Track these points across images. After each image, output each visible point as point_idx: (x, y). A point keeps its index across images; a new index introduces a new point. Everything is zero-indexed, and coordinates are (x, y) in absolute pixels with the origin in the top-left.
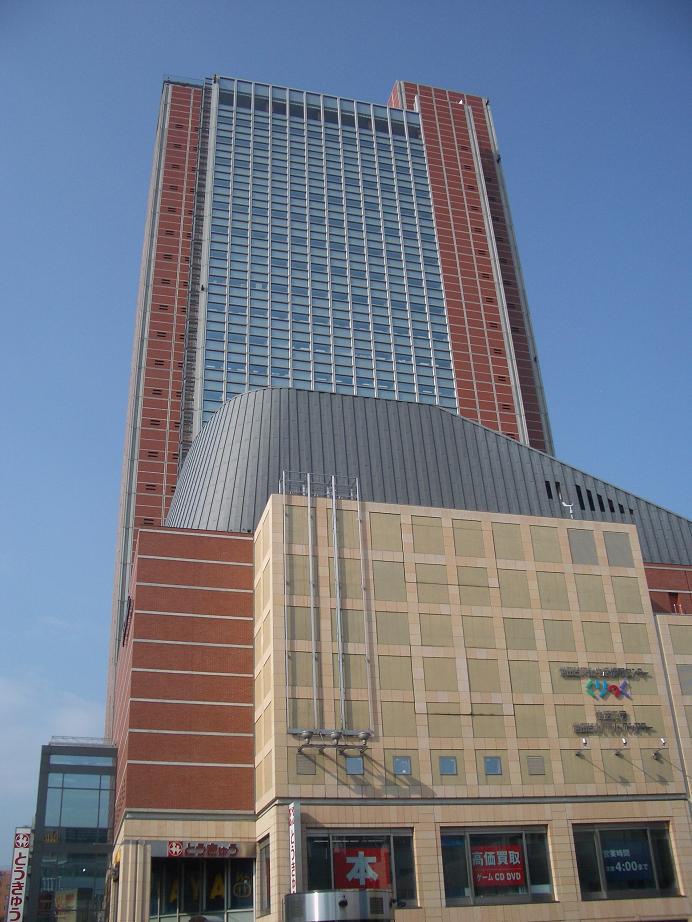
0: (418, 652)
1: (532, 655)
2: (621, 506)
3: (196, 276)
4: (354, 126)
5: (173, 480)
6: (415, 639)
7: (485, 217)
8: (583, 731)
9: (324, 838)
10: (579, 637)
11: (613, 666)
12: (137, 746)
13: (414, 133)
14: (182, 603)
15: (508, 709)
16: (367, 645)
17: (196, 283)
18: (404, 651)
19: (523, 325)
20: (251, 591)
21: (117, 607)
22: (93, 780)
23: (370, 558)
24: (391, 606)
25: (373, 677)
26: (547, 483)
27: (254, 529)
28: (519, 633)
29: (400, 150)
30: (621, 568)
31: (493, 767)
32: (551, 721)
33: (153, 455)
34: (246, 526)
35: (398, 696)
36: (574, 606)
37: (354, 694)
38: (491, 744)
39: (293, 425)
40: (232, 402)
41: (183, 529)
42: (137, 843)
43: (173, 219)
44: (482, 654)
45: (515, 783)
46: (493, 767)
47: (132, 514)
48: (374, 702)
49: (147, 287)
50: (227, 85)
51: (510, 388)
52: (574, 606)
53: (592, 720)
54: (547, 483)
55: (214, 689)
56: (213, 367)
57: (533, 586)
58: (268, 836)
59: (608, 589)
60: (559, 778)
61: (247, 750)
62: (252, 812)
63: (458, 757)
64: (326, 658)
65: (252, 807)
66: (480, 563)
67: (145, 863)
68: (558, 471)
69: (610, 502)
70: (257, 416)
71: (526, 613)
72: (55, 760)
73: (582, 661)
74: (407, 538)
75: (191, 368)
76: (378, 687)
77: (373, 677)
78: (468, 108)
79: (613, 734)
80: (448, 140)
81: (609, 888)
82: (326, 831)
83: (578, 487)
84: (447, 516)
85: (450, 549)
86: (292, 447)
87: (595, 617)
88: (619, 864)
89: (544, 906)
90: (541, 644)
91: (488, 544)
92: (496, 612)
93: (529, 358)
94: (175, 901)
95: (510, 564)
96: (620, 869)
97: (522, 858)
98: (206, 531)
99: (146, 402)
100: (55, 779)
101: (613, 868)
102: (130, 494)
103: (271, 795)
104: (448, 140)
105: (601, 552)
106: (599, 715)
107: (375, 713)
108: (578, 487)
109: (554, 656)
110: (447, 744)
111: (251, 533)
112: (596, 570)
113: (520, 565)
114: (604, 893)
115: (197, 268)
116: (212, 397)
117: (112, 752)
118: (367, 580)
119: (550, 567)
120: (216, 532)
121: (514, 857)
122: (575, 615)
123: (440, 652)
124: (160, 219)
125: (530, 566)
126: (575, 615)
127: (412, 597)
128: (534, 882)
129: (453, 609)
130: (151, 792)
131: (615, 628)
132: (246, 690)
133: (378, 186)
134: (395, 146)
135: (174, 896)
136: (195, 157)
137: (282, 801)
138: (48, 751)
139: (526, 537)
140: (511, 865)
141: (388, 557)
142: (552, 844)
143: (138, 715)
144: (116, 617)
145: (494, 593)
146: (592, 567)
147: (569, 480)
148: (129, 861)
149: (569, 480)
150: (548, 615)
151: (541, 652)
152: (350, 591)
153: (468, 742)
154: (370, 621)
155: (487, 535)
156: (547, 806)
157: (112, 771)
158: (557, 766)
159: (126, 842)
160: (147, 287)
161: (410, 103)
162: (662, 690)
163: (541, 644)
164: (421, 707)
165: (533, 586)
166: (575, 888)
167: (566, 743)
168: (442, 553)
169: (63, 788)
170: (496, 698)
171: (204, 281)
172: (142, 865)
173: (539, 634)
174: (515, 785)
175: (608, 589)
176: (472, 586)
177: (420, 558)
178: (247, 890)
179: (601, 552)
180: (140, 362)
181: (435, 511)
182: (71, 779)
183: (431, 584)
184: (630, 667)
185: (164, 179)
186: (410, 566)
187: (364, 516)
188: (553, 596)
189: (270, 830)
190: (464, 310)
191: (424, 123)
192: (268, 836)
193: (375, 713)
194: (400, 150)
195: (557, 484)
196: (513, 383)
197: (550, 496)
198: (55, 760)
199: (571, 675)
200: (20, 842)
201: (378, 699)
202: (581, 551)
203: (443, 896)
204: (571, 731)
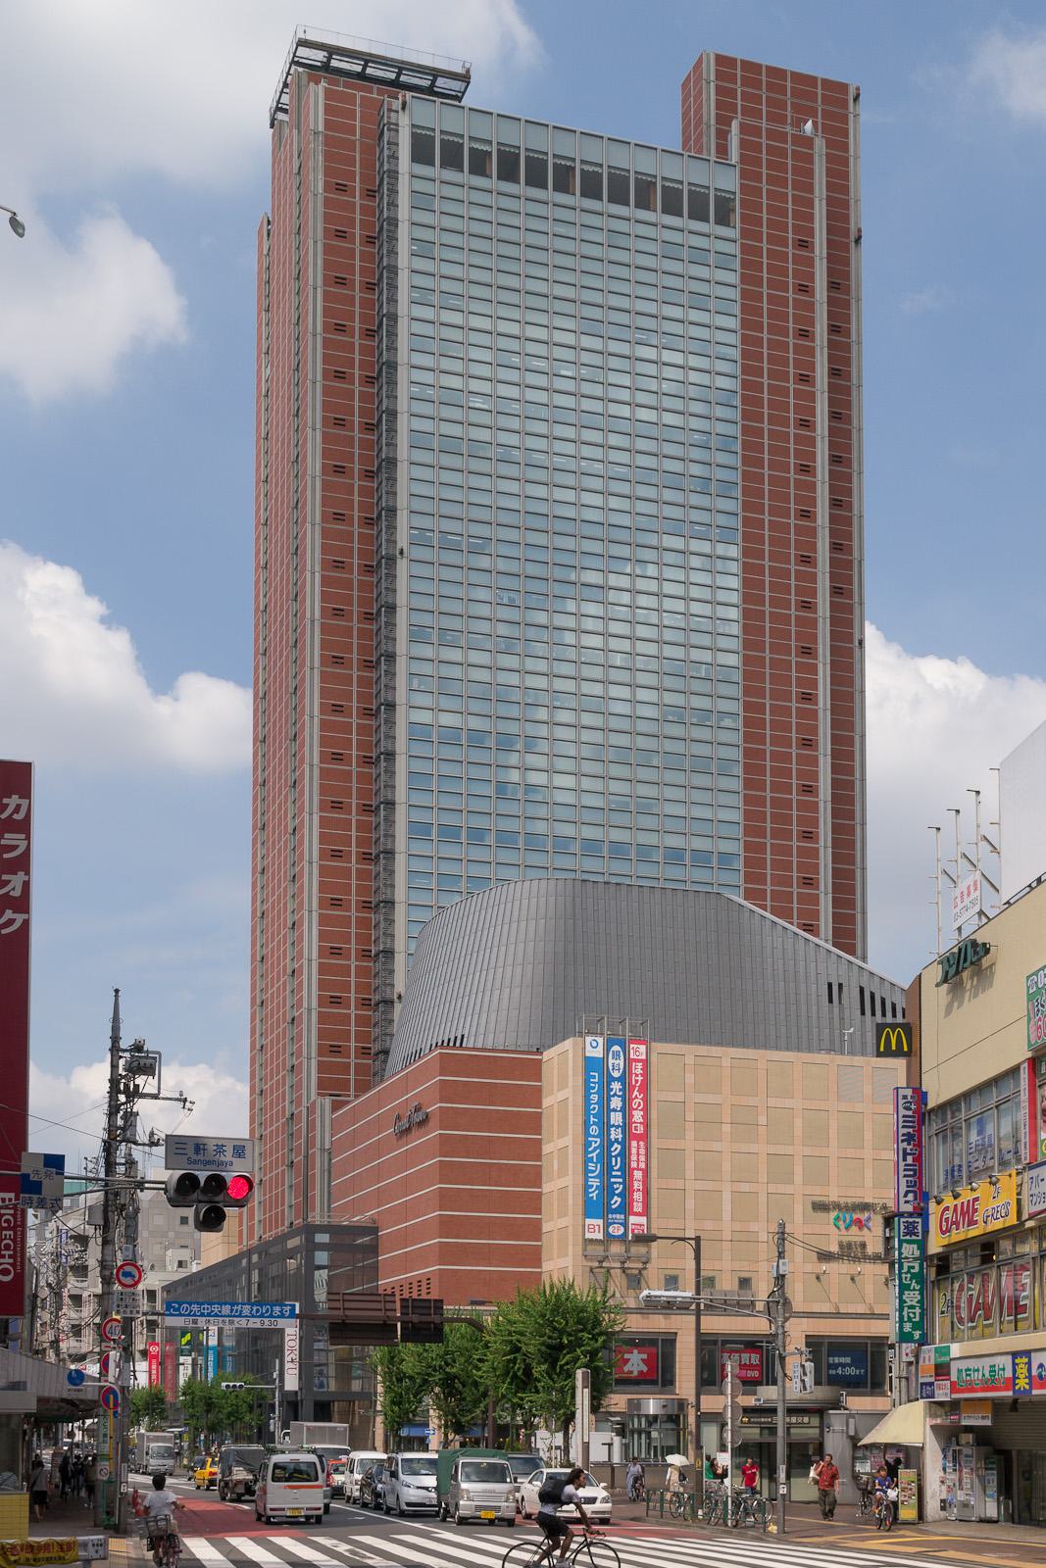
6: (690, 1173)
8: (825, 1256)
11: (861, 1200)
18: (680, 1184)
26: (830, 985)
44: (745, 1187)
54: (830, 985)
55: (507, 1202)
71: (788, 1150)
73: (834, 1195)
74: (690, 1078)
87: (851, 1153)
97: (761, 1360)
123: (709, 1186)
127: (690, 1134)
150: (808, 1151)
167: (809, 1268)
170: (754, 1227)
177: (700, 1098)
197: (831, 1001)
199: (820, 1207)
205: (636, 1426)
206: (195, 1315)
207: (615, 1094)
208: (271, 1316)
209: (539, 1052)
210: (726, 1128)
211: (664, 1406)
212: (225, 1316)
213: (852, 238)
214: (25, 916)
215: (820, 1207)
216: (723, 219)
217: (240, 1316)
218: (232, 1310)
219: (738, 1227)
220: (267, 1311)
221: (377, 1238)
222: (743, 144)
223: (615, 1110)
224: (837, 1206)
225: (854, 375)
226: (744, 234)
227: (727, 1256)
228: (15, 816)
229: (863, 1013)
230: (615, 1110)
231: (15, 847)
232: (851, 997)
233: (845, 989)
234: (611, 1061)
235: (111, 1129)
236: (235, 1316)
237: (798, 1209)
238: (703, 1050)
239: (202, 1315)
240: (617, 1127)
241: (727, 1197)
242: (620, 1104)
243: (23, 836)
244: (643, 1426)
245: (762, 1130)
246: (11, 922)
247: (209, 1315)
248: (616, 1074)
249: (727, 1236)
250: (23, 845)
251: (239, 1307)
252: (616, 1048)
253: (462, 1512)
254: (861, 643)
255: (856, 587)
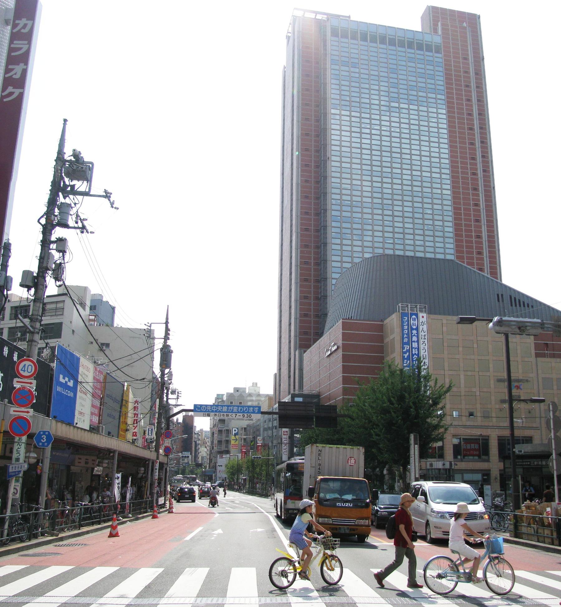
15: (478, 394)
19: (482, 84)
26: (498, 295)
44: (469, 373)
45: (479, 421)
51: (475, 148)
54: (498, 295)
93: (490, 187)
97: (479, 447)
121: (477, 446)
140: (475, 449)
162: (536, 387)
167: (497, 406)
184: (524, 378)
196: (484, 239)
206: (209, 411)
207: (414, 335)
208: (248, 412)
209: (382, 321)
210: (461, 349)
212: (224, 412)
214: (21, 90)
216: (437, 52)
217: (232, 412)
218: (228, 409)
220: (246, 410)
221: (319, 399)
222: (443, 29)
223: (414, 342)
226: (445, 55)
228: (23, 31)
229: (512, 305)
230: (414, 342)
231: (20, 49)
232: (507, 300)
234: (412, 322)
235: (49, 214)
236: (229, 412)
237: (492, 382)
239: (213, 411)
240: (415, 348)
241: (462, 377)
242: (416, 339)
243: (26, 42)
246: (11, 94)
247: (216, 411)
248: (414, 327)
249: (463, 394)
250: (25, 48)
251: (232, 408)
252: (414, 317)
254: (494, 188)
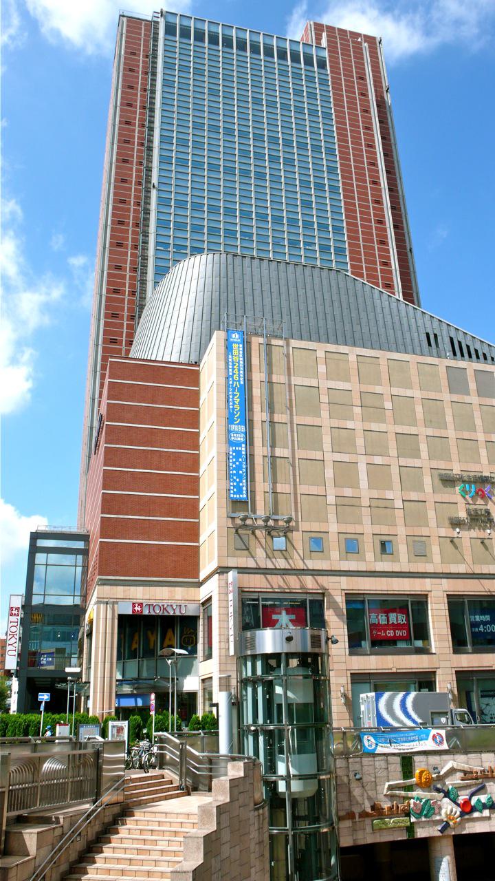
0: (330, 457)
1: (417, 463)
2: (484, 355)
3: (149, 176)
4: (274, 57)
5: (131, 335)
6: (327, 446)
7: (375, 135)
8: (456, 523)
9: (253, 600)
10: (454, 450)
11: (480, 474)
12: (107, 527)
13: (322, 65)
14: (141, 414)
16: (290, 450)
17: (148, 181)
18: (318, 455)
20: (198, 409)
21: (87, 432)
22: (69, 559)
23: (293, 383)
24: (308, 420)
25: (294, 475)
26: (428, 335)
27: (200, 360)
28: (407, 444)
29: (310, 79)
30: (487, 399)
31: (384, 547)
32: (431, 514)
33: (115, 316)
34: (193, 359)
35: (314, 490)
36: (450, 426)
37: (280, 488)
38: (384, 530)
39: (230, 281)
40: (178, 266)
41: (143, 360)
42: (107, 604)
43: (129, 130)
44: (378, 460)
46: (384, 547)
47: (101, 327)
48: (295, 494)
49: (110, 184)
50: (171, 19)
52: (450, 426)
53: (463, 514)
54: (428, 335)
55: (167, 484)
56: (162, 248)
57: (419, 409)
58: (210, 599)
59: (477, 414)
60: (437, 558)
61: (193, 532)
62: (196, 580)
63: (359, 540)
64: (258, 460)
65: (197, 576)
66: (378, 389)
67: (113, 619)
68: (436, 324)
69: (476, 351)
70: (202, 274)
71: (413, 430)
72: (42, 543)
73: (457, 469)
74: (322, 369)
75: (145, 249)
76: (298, 483)
77: (294, 475)
78: (365, 45)
79: (479, 529)
80: (348, 73)
81: (474, 644)
82: (257, 594)
83: (451, 339)
84: (353, 353)
85: (355, 378)
86: (229, 284)
87: (466, 435)
88: (482, 626)
89: (425, 657)
90: (424, 453)
91: (385, 376)
92: (391, 428)
94: (136, 649)
95: (402, 392)
96: (482, 630)
97: (408, 620)
98: (162, 362)
99: (109, 275)
100: (40, 558)
101: (477, 629)
102: (97, 346)
103: (214, 565)
104: (348, 73)
105: (472, 386)
106: (468, 511)
107: (296, 503)
108: (451, 339)
109: (435, 464)
110: (350, 528)
111: (197, 364)
112: (467, 399)
113: (409, 393)
114: (469, 648)
115: (149, 170)
116: (162, 272)
117: (85, 538)
118: (291, 400)
119: (432, 395)
120: (169, 363)
122: (451, 433)
123: (345, 458)
124: (112, 231)
125: (417, 394)
126: (451, 433)
127: (325, 414)
128: (416, 638)
129: (356, 424)
130: (116, 565)
131: (482, 445)
132: (193, 485)
133: (292, 108)
134: (306, 75)
135: (135, 646)
136: (146, 80)
137: (222, 570)
138: (35, 536)
139: (413, 370)
140: (399, 624)
141: (307, 382)
142: (432, 616)
143: (108, 504)
144: (87, 439)
145: (389, 413)
146: (465, 397)
147: (445, 333)
148: (100, 620)
149: (445, 333)
150: (430, 432)
151: (424, 460)
152: (277, 407)
153: (367, 528)
154: (292, 431)
155: (384, 369)
156: (428, 581)
157: (85, 552)
158: (435, 549)
159: (98, 603)
160: (110, 184)
161: (319, 39)
163: (424, 453)
164: (331, 499)
165: (419, 409)
166: (448, 643)
167: (443, 532)
168: (348, 380)
169: (47, 565)
170: (389, 495)
171: (155, 180)
172: (109, 679)
173: (423, 447)
174: (404, 565)
175: (477, 414)
176: (372, 407)
177: (332, 384)
178: (192, 641)
179: (472, 386)
180: (115, 122)
181: (343, 349)
182: (53, 558)
183: (340, 405)
185: (118, 153)
186: (323, 391)
187: (288, 350)
188: (435, 417)
189: (213, 594)
190: (368, 179)
191: (330, 56)
192: (210, 599)
193: (296, 503)
194: (310, 79)
195: (436, 336)
197: (430, 344)
198: (42, 543)
199: (448, 481)
200: (13, 612)
201: (298, 492)
202: (456, 382)
203: (347, 647)
204: (447, 523)
205: (249, 674)
211: (289, 639)
213: (385, 89)
215: (448, 481)
219: (375, 494)
224: (461, 480)
225: (392, 138)
227: (367, 520)
233: (439, 338)
238: (332, 347)
244: (259, 672)
245: (389, 413)
253: (241, 764)
255: (405, 225)
